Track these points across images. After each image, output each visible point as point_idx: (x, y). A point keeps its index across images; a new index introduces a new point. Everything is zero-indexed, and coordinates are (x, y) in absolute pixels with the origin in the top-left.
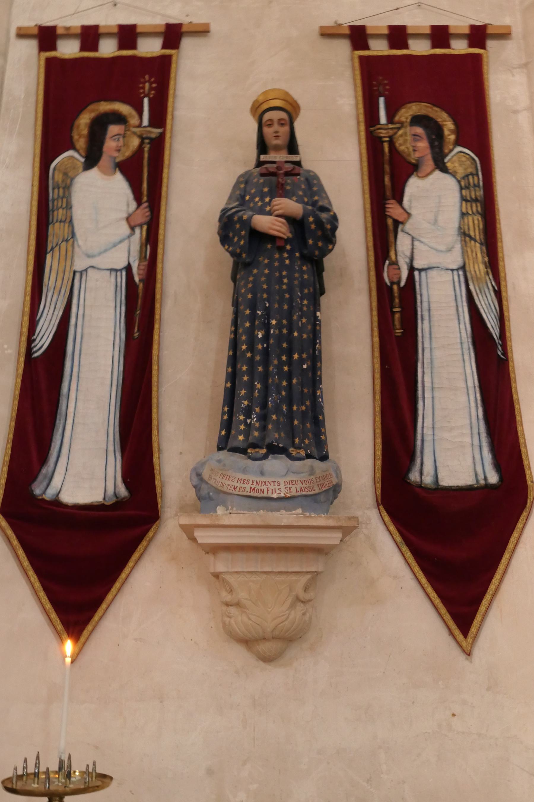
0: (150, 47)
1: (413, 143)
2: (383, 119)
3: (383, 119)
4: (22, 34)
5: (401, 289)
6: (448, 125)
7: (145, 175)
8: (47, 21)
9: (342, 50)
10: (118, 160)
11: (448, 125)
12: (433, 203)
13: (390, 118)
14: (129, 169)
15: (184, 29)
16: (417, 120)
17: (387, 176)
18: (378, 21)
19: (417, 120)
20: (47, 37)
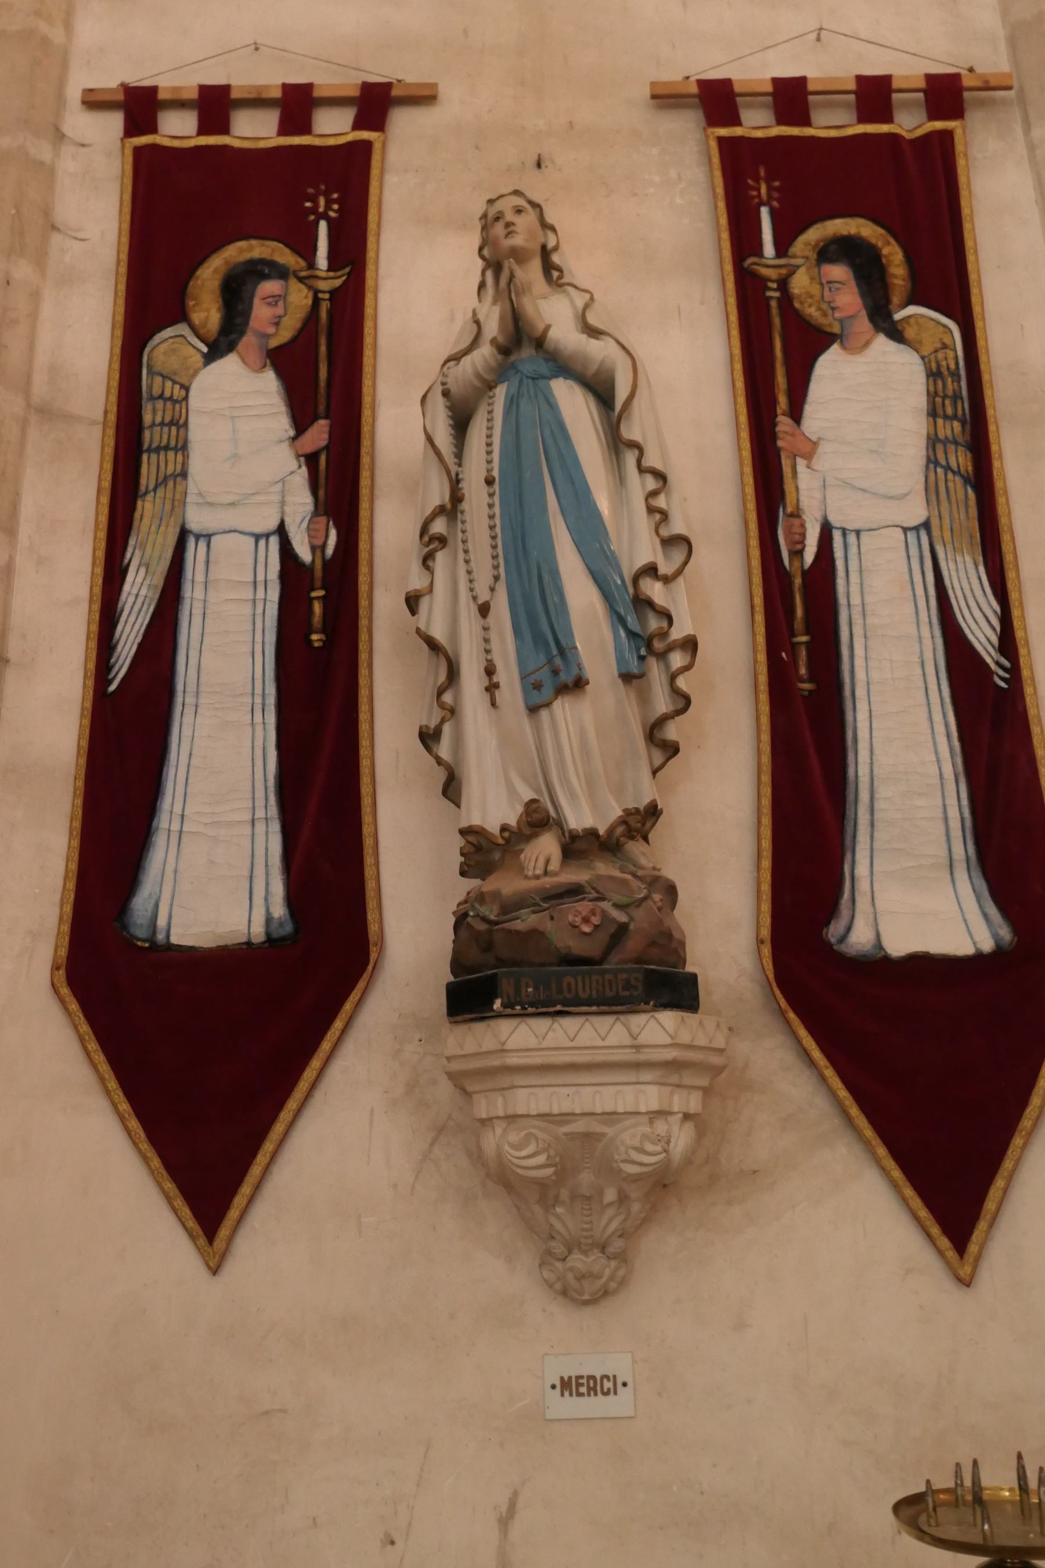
0: (333, 126)
1: (828, 291)
2: (769, 249)
3: (769, 249)
4: (94, 102)
5: (805, 574)
6: (893, 255)
7: (323, 349)
8: (139, 77)
9: (687, 128)
10: (274, 343)
11: (893, 255)
12: (868, 401)
13: (782, 248)
14: (290, 363)
15: (395, 92)
16: (826, 253)
17: (775, 358)
18: (755, 69)
19: (826, 253)
20: (139, 107)
